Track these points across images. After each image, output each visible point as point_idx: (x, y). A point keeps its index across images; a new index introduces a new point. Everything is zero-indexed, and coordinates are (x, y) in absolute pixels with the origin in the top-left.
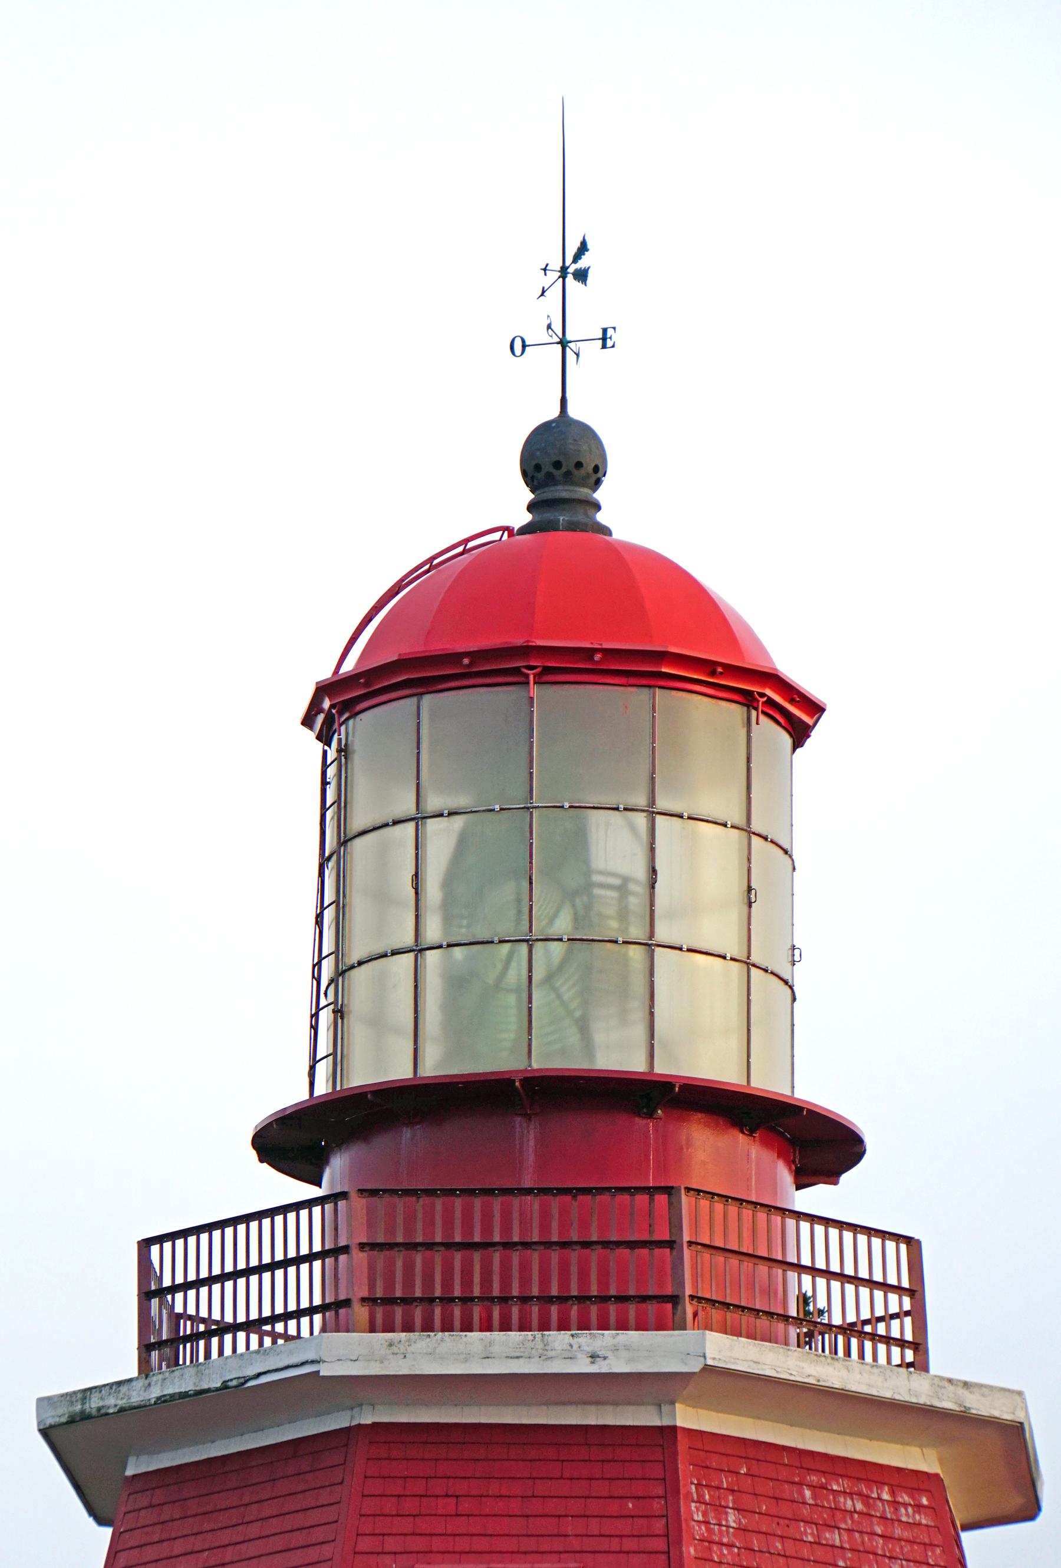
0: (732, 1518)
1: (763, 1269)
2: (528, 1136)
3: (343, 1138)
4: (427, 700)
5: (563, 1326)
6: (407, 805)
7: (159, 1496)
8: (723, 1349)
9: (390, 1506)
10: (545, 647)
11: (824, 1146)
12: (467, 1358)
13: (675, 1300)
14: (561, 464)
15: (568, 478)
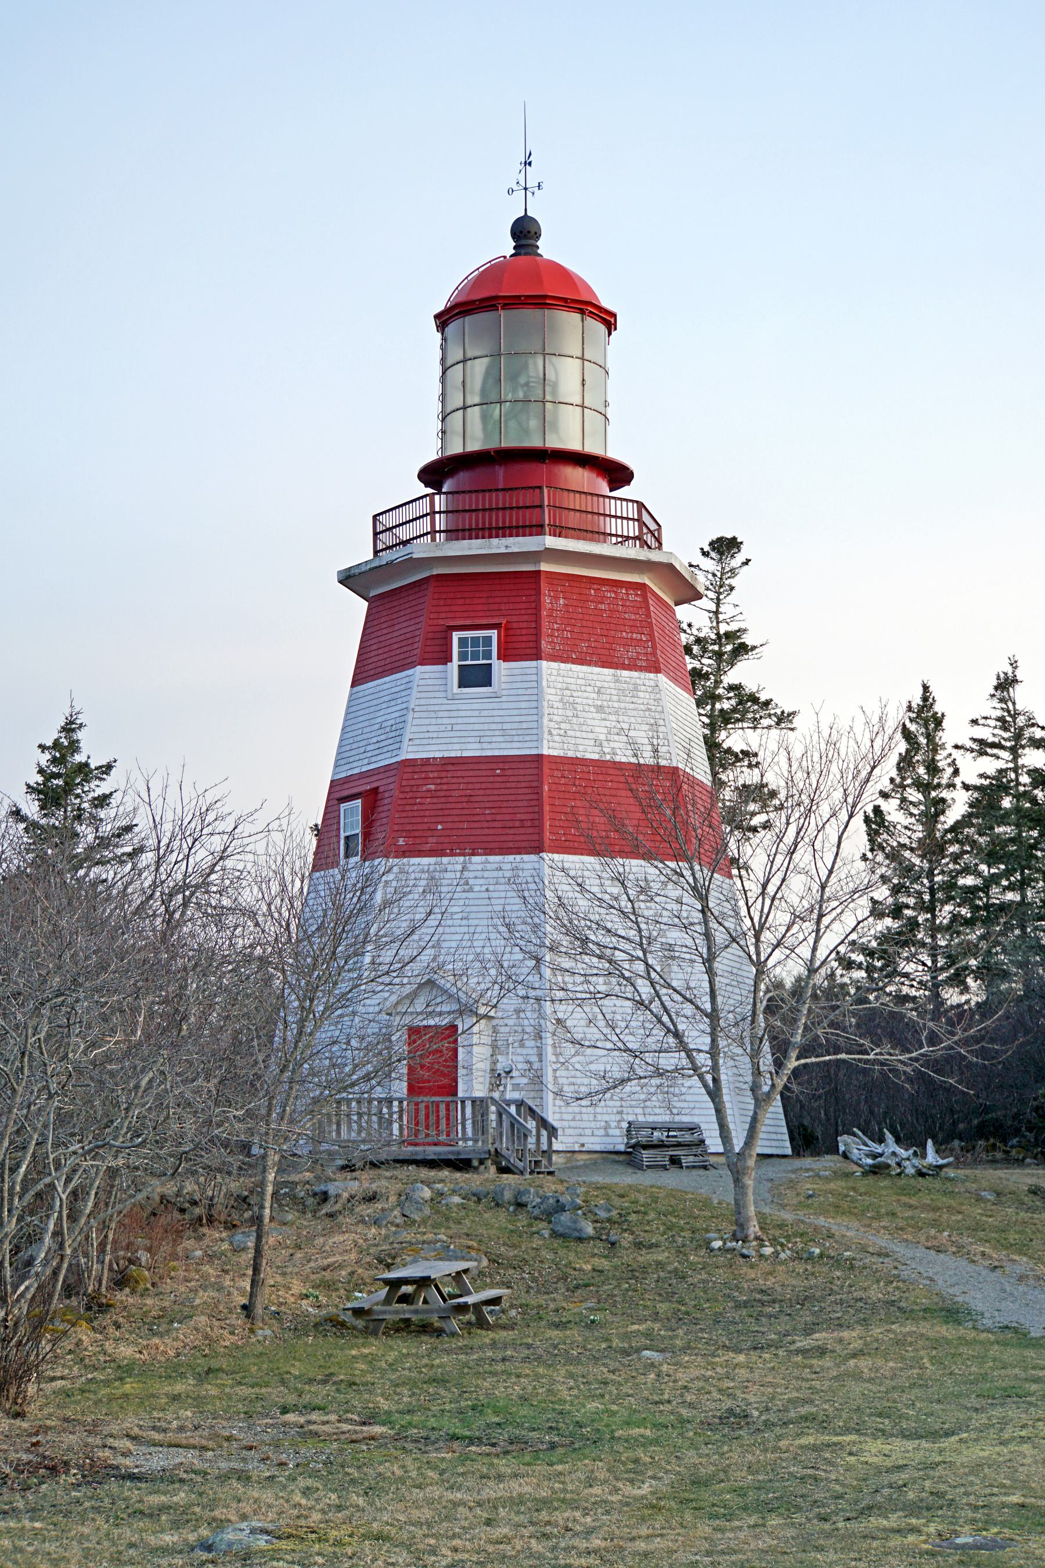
0: (562, 601)
1: (590, 516)
2: (500, 472)
3: (451, 474)
4: (467, 318)
5: (497, 536)
6: (460, 357)
7: (379, 603)
8: (551, 542)
9: (442, 602)
10: (516, 299)
11: (618, 474)
12: (463, 549)
13: (542, 526)
14: (525, 232)
15: (526, 237)
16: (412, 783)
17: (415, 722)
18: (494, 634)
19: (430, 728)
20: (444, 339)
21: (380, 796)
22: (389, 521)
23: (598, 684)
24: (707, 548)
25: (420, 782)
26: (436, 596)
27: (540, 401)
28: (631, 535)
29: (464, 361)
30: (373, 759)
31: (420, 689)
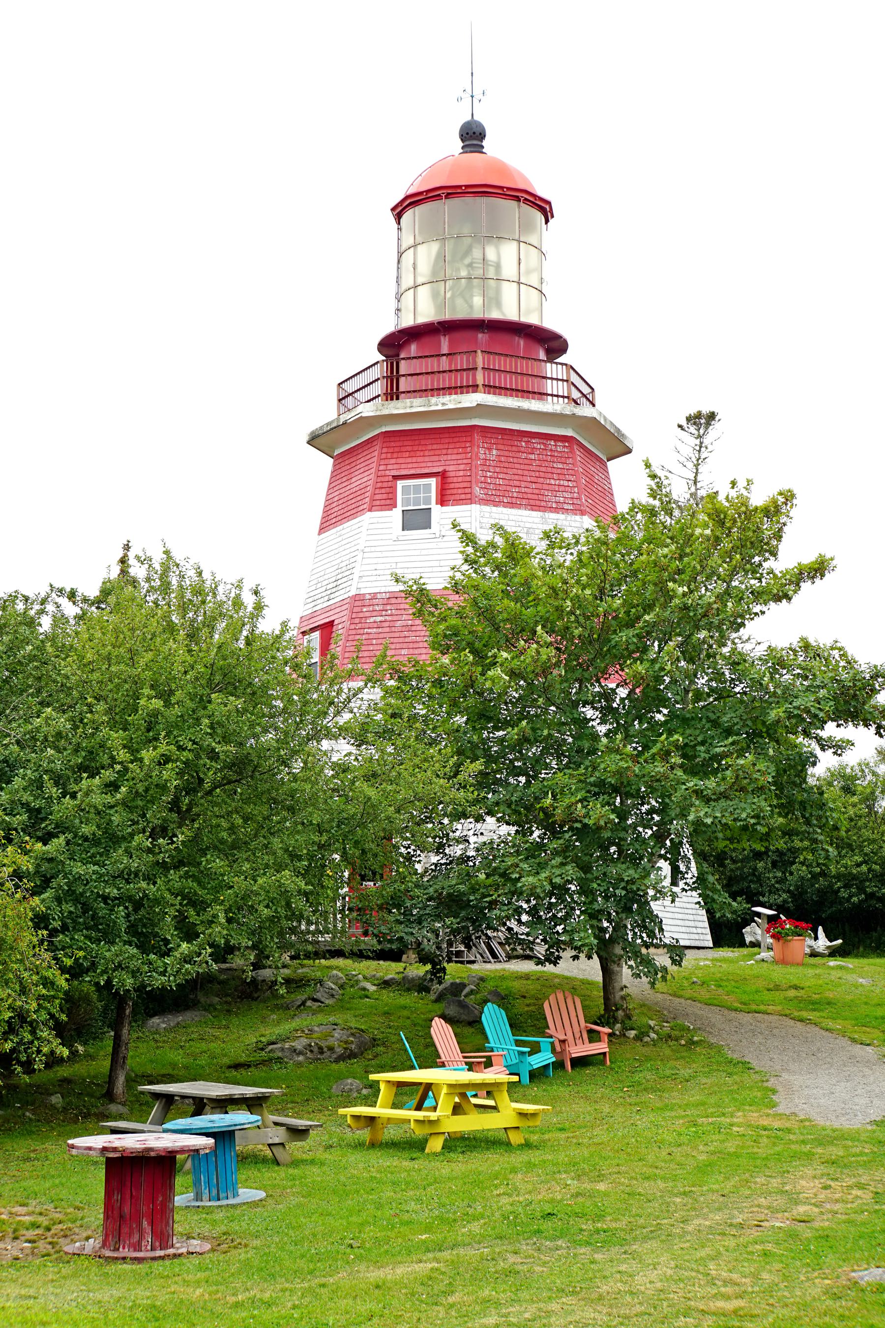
0: (494, 452)
11: (554, 345)
14: (473, 136)
16: (361, 615)
17: (366, 561)
18: (433, 482)
19: (378, 567)
20: (400, 229)
21: (334, 628)
22: (350, 387)
23: (528, 525)
24: (684, 423)
25: (367, 614)
26: (385, 450)
27: (487, 279)
28: (561, 394)
29: (415, 246)
30: (332, 596)
31: (370, 532)
